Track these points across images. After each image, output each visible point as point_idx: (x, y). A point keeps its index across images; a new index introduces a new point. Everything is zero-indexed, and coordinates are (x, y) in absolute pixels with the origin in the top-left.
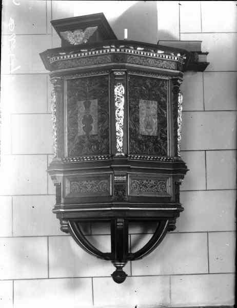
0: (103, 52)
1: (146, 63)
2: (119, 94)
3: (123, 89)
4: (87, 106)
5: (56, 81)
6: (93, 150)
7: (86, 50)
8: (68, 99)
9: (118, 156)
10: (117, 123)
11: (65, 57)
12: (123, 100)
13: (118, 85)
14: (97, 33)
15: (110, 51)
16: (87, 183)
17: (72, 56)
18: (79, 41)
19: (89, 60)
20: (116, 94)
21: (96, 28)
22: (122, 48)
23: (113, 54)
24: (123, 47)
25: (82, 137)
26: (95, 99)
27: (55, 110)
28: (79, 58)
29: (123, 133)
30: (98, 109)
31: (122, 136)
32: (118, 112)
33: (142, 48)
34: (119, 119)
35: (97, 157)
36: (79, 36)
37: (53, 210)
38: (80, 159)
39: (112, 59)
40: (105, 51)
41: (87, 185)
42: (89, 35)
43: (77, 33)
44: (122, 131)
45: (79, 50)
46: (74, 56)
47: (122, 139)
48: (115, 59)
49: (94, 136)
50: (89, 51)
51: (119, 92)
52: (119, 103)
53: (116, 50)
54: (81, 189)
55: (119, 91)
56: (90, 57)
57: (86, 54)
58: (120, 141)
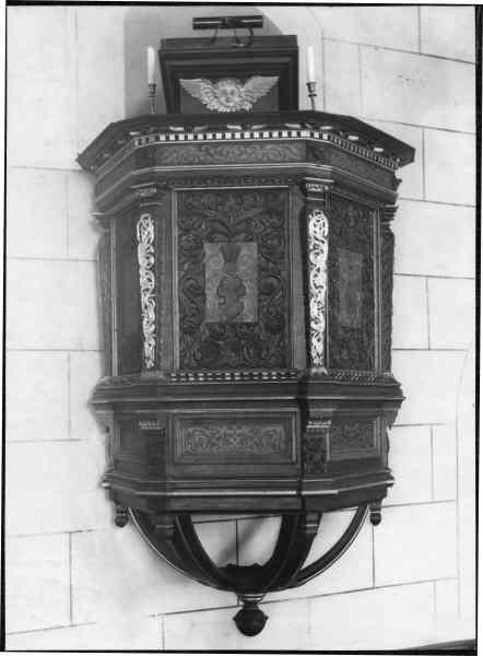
0: (224, 137)
1: (216, 157)
2: (318, 236)
3: (327, 225)
4: (231, 258)
5: (155, 191)
6: (247, 357)
7: (239, 128)
8: (180, 236)
9: (316, 374)
10: (312, 300)
11: (181, 137)
12: (325, 247)
13: (317, 214)
14: (277, 89)
15: (299, 134)
16: (231, 432)
17: (200, 136)
18: (231, 104)
19: (242, 148)
20: (311, 232)
21: (276, 78)
22: (325, 131)
23: (307, 142)
24: (329, 131)
25: (216, 327)
26: (251, 240)
27: (152, 260)
28: (220, 144)
29: (323, 323)
30: (259, 265)
31: (322, 330)
32: (316, 276)
33: (202, 125)
34: (317, 291)
35: (251, 374)
36: (232, 93)
37: (391, 485)
38: (214, 376)
39: (301, 156)
40: (228, 135)
41: (230, 435)
42: (257, 95)
43: (228, 86)
44: (322, 317)
45: (164, 128)
46: (271, 136)
47: (321, 336)
48: (310, 156)
49: (248, 325)
50: (245, 129)
51: (317, 229)
52: (317, 254)
53: (312, 135)
54: (214, 444)
55: (318, 226)
56: (247, 144)
57: (238, 135)
58: (319, 340)
